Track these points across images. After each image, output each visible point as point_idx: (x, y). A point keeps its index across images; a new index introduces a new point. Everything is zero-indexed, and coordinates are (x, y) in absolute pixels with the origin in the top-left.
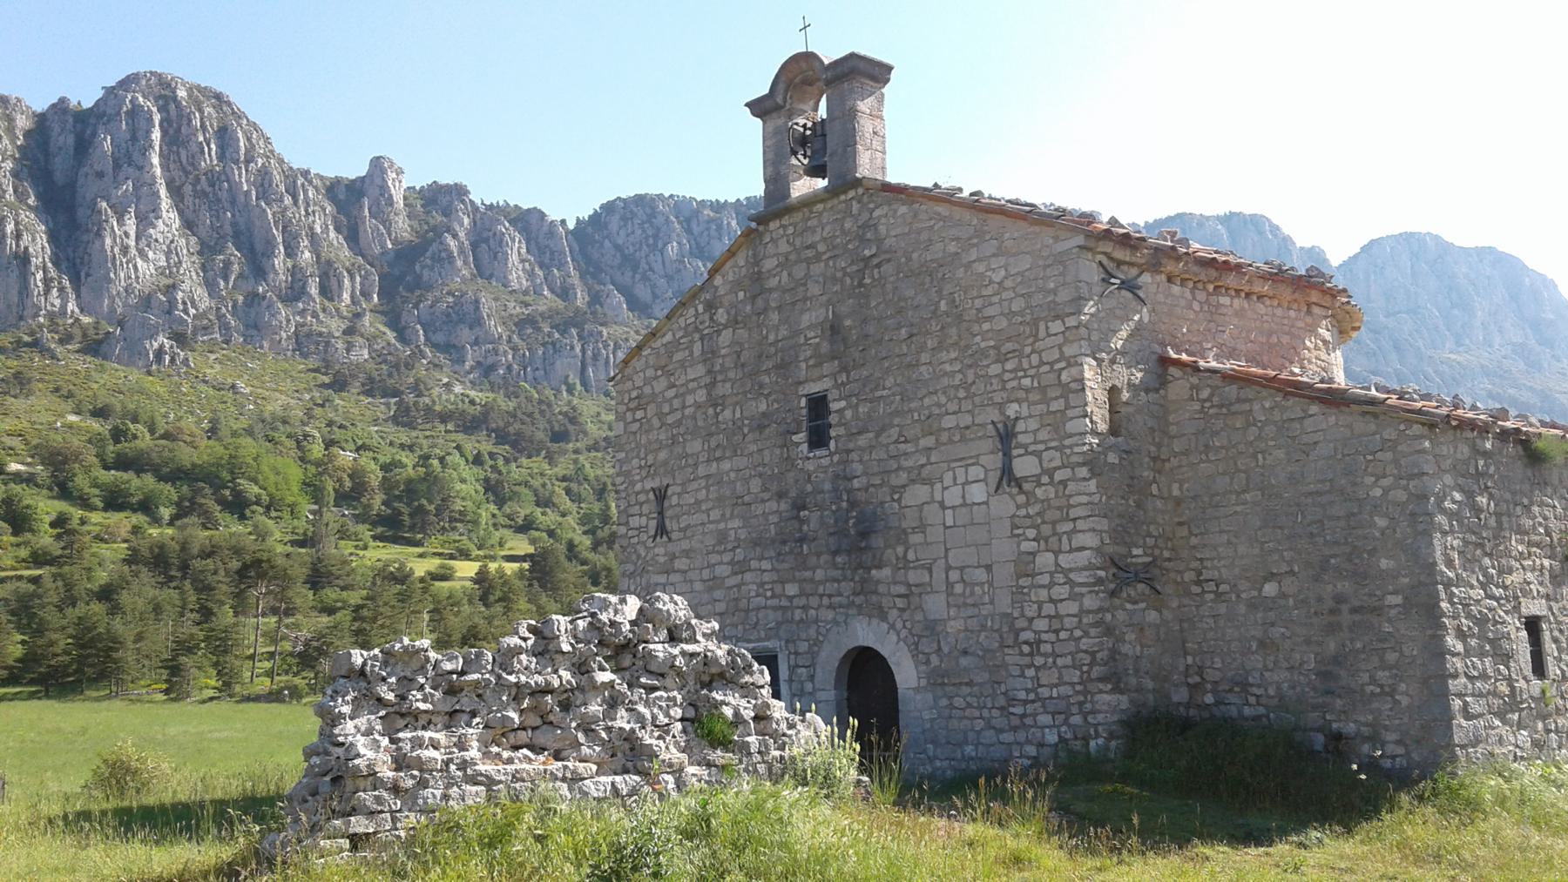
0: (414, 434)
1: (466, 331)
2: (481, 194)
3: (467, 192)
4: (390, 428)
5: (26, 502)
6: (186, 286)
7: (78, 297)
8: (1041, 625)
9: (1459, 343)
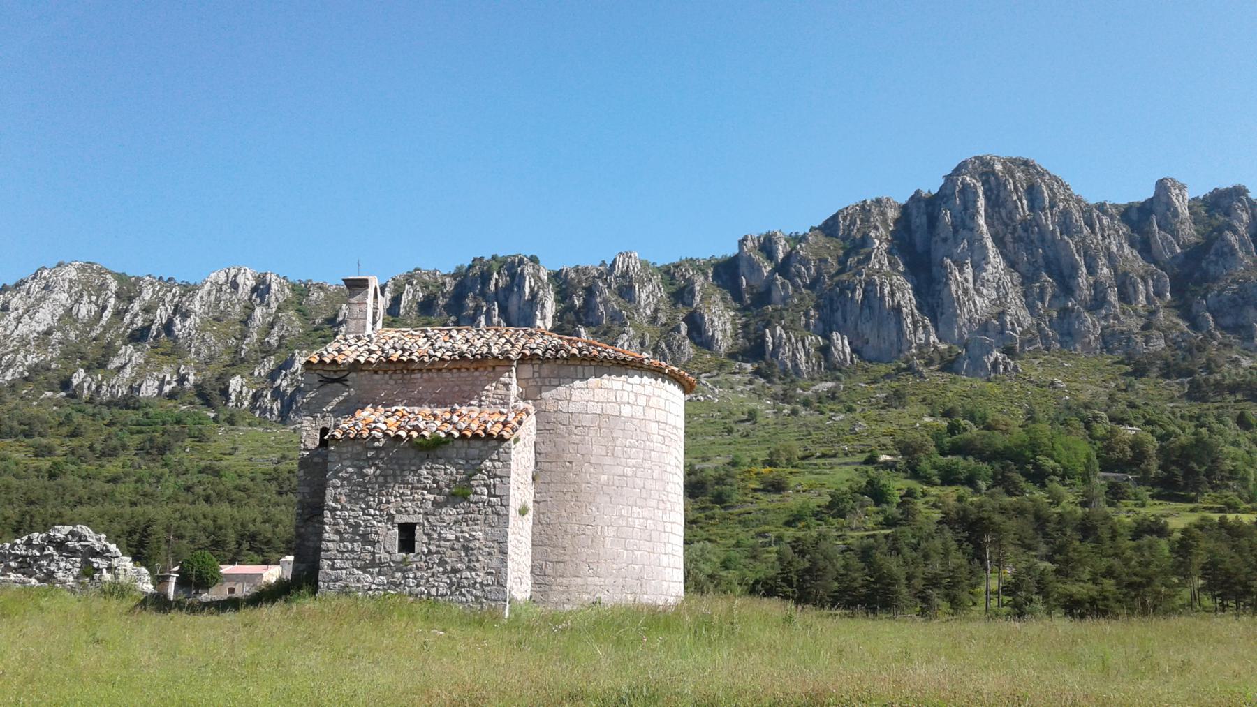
0: (1205, 406)
4: (1186, 403)
5: (882, 482)
6: (1012, 311)
7: (937, 331)
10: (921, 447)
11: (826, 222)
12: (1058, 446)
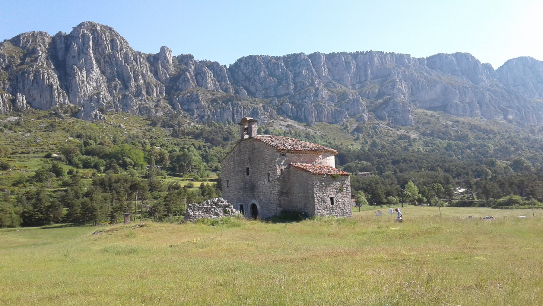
0: (179, 140)
1: (194, 105)
2: (198, 57)
3: (193, 57)
5: (60, 166)
6: (103, 93)
7: (69, 98)
9: (540, 95)
10: (73, 151)
11: (13, 39)
12: (132, 153)
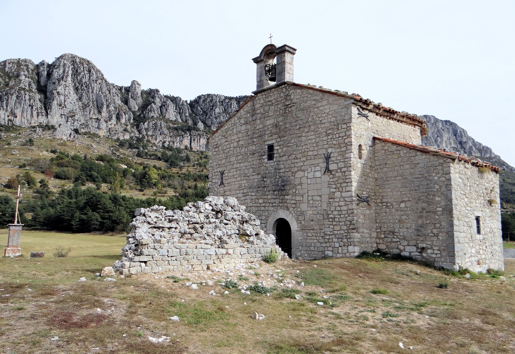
2: (164, 92)
8: (336, 213)
